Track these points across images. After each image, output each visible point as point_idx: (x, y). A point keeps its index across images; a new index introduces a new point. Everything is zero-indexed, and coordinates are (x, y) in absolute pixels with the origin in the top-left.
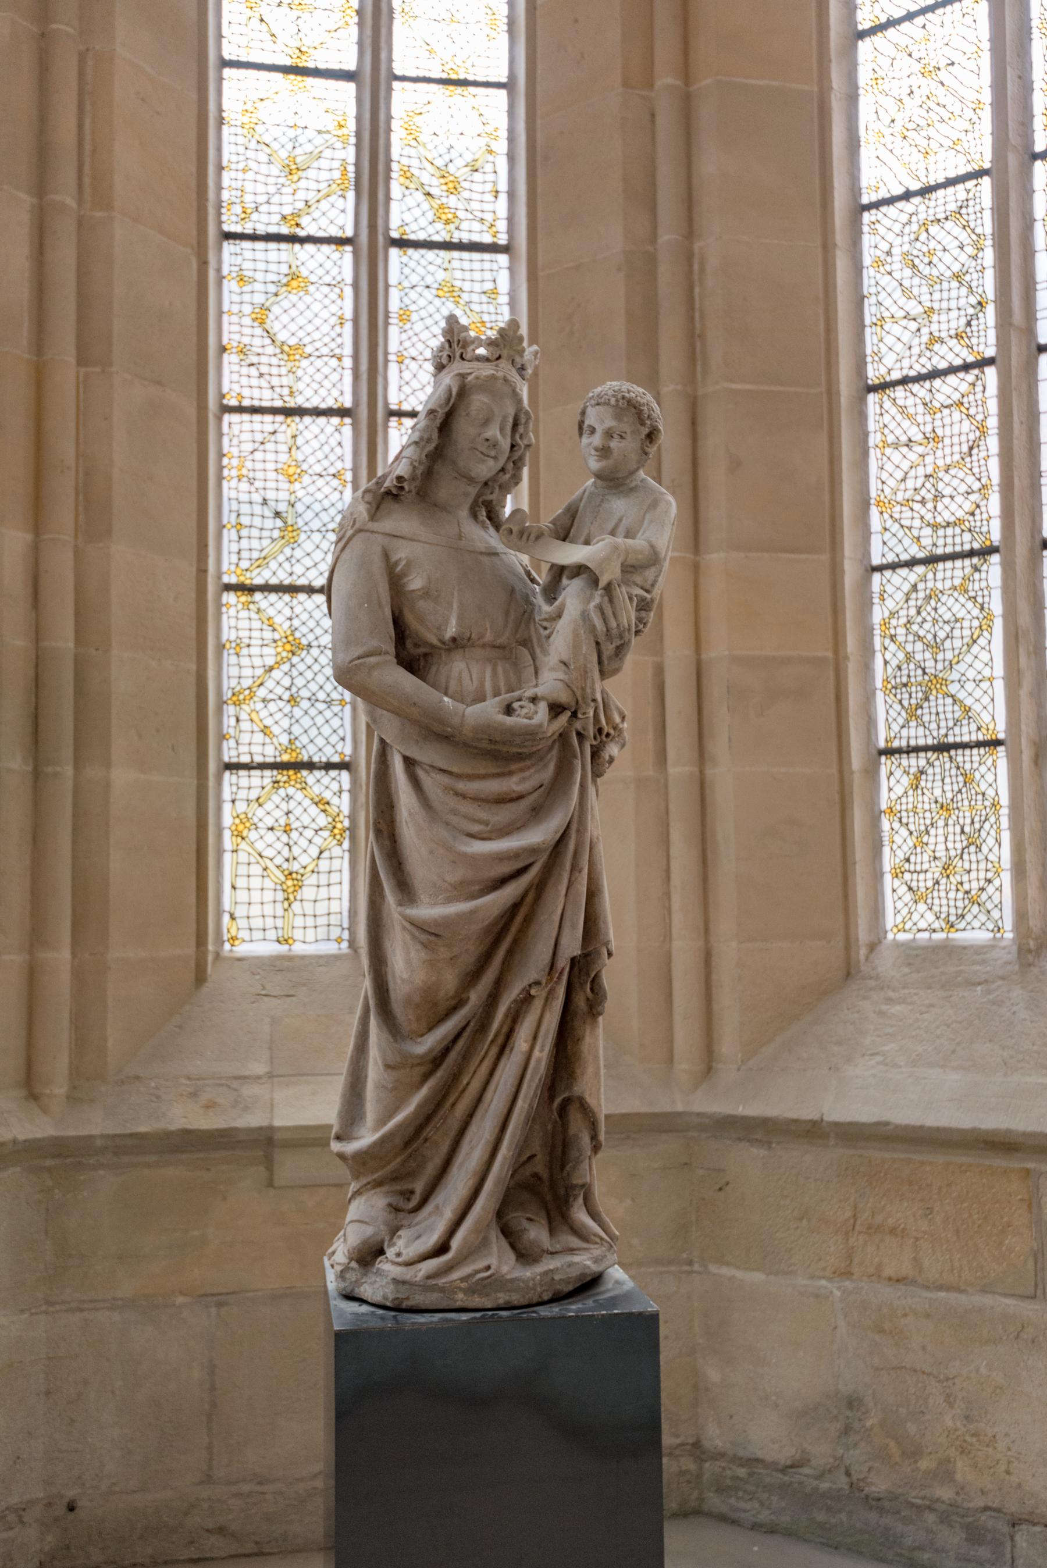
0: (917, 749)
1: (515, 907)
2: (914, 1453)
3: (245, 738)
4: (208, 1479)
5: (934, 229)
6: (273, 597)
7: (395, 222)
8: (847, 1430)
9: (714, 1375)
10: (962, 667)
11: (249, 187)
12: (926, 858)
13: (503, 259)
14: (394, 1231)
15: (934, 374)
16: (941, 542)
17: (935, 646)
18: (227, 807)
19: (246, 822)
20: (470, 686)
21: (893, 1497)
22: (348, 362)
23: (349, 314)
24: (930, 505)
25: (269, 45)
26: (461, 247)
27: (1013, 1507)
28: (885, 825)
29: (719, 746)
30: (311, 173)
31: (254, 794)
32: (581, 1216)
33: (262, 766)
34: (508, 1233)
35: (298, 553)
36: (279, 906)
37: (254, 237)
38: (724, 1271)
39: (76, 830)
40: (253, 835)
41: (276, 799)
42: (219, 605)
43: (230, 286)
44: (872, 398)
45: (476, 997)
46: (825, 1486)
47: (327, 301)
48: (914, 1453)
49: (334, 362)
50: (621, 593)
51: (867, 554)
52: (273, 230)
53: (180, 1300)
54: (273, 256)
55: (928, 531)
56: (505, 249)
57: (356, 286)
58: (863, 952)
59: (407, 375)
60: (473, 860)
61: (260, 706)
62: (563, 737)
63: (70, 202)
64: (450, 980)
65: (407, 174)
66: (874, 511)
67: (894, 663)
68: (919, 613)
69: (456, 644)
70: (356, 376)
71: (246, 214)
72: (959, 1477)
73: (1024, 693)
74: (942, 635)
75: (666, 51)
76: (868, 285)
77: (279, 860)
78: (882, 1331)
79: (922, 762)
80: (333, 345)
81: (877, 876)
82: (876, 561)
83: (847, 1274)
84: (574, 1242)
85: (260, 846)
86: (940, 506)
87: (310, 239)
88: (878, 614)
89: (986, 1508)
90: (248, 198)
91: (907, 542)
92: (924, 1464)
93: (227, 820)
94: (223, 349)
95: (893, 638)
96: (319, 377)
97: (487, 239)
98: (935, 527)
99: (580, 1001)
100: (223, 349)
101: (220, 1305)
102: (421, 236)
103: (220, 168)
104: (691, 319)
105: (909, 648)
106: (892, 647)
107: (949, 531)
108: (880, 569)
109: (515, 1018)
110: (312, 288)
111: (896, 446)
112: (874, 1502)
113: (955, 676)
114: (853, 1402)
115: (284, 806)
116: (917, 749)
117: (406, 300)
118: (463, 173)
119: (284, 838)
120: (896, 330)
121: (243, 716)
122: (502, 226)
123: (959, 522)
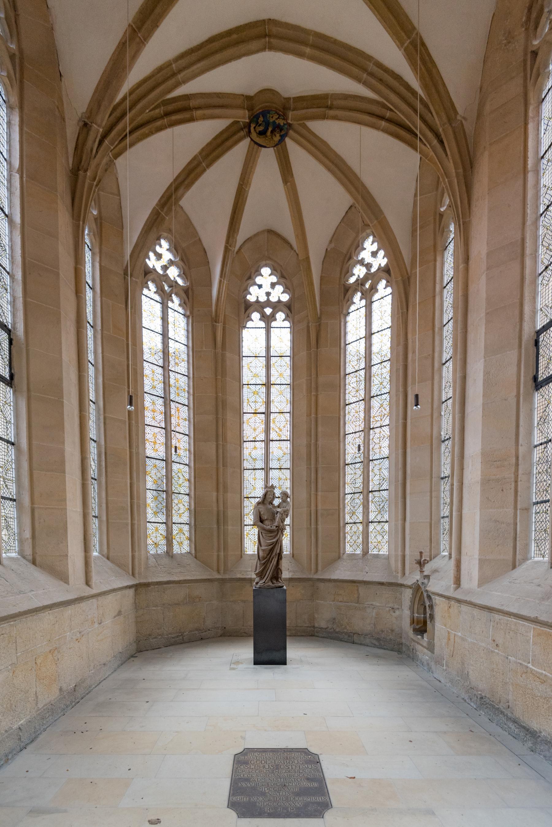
0: (351, 523)
1: (272, 548)
4: (243, 626)
5: (356, 439)
6: (252, 499)
7: (271, 437)
8: (334, 623)
9: (316, 616)
11: (248, 433)
13: (289, 442)
15: (356, 463)
17: (354, 507)
18: (245, 531)
20: (268, 524)
21: (339, 632)
22: (263, 461)
23: (264, 453)
25: (251, 409)
26: (282, 440)
27: (354, 632)
28: (346, 535)
29: (319, 523)
30: (258, 430)
32: (280, 580)
33: (250, 525)
34: (272, 582)
35: (256, 492)
37: (249, 441)
38: (318, 601)
39: (224, 535)
40: (249, 536)
42: (244, 500)
43: (245, 449)
44: (347, 466)
45: (268, 557)
50: (283, 514)
51: (345, 492)
52: (252, 440)
54: (252, 444)
56: (289, 440)
57: (265, 448)
58: (342, 555)
60: (268, 543)
62: (278, 529)
63: (221, 443)
64: (265, 555)
65: (273, 429)
66: (346, 485)
69: (266, 519)
70: (265, 463)
73: (365, 516)
75: (313, 410)
76: (346, 448)
81: (345, 543)
82: (346, 493)
83: (334, 601)
87: (258, 441)
88: (346, 501)
90: (248, 435)
93: (245, 533)
97: (286, 439)
98: (355, 488)
99: (280, 558)
102: (275, 439)
103: (243, 430)
104: (316, 455)
108: (347, 494)
109: (272, 559)
111: (350, 474)
112: (337, 633)
114: (334, 619)
116: (351, 523)
118: (282, 428)
120: (350, 455)
122: (289, 436)
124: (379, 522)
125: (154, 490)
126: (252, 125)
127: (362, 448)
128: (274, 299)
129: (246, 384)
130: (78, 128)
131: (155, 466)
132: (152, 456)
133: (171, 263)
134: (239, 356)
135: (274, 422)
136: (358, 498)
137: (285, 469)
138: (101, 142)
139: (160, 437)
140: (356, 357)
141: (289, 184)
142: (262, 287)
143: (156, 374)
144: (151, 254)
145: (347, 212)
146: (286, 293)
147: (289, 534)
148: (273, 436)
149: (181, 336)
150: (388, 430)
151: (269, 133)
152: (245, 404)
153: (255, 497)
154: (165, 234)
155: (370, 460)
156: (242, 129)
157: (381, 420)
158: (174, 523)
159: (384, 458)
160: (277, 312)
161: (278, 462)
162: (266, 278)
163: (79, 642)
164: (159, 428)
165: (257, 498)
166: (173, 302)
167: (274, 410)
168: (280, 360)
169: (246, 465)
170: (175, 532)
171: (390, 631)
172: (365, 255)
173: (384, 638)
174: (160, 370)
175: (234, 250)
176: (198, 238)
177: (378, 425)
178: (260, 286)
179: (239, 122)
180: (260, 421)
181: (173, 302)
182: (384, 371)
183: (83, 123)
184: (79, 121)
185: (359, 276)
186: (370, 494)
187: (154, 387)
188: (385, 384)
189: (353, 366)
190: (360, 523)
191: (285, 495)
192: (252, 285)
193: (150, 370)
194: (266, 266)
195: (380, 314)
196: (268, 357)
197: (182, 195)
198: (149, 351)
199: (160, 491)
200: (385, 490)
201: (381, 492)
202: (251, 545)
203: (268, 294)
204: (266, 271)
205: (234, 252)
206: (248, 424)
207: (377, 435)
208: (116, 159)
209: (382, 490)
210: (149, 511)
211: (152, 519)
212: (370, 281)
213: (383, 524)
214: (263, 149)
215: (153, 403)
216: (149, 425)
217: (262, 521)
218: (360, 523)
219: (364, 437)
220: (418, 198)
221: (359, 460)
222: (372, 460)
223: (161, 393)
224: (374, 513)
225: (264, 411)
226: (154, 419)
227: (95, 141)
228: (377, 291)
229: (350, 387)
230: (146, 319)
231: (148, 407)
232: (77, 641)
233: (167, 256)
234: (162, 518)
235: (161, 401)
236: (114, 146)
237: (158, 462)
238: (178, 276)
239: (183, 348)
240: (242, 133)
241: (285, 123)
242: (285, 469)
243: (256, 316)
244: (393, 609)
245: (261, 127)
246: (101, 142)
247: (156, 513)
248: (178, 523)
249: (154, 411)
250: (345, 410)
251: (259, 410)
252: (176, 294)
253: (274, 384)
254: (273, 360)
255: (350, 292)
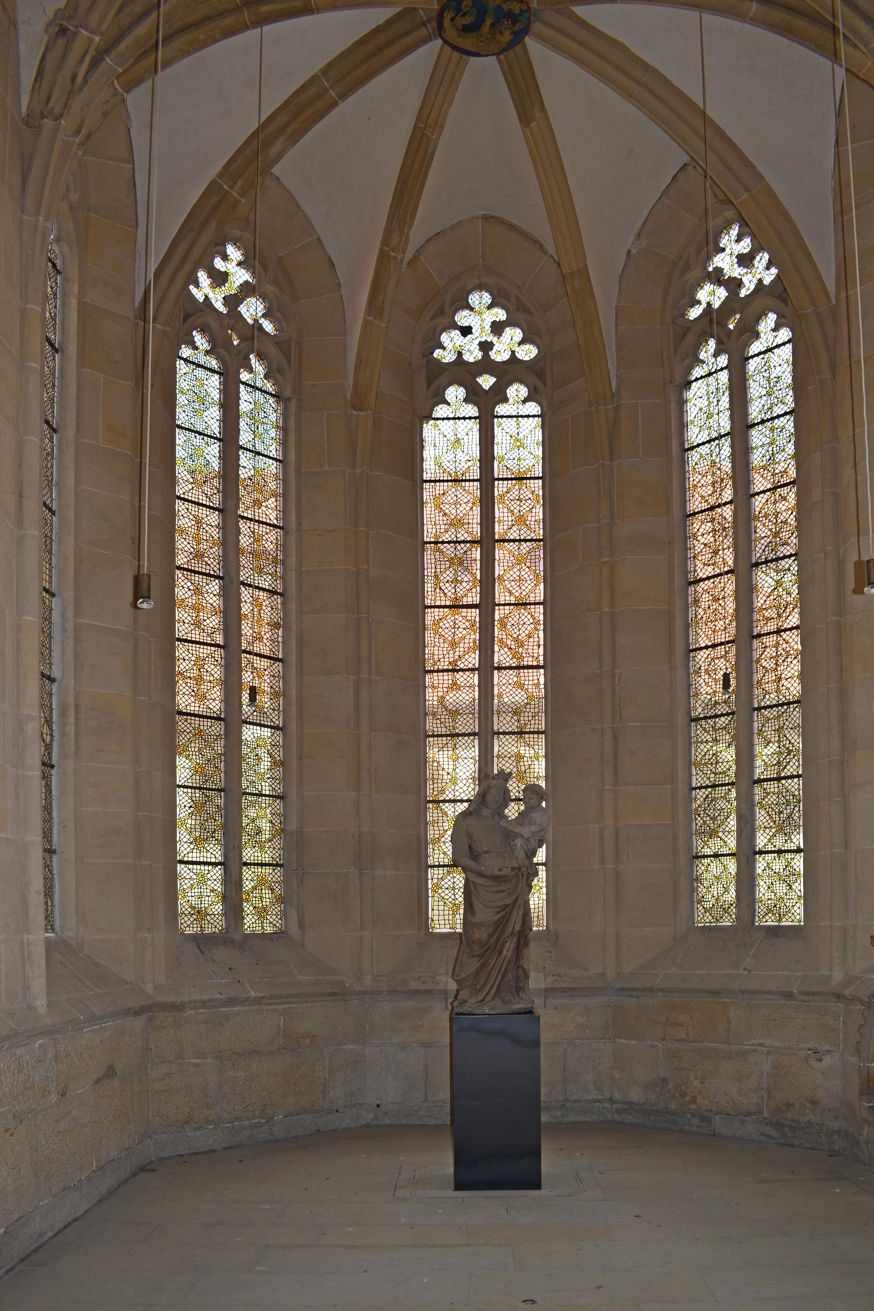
1: (502, 918)
2: (683, 1095)
3: (436, 856)
10: (724, 826)
11: (436, 652)
12: (710, 896)
14: (470, 998)
15: (716, 716)
16: (717, 780)
17: (714, 819)
18: (430, 881)
19: (437, 886)
24: (714, 766)
25: (443, 598)
30: (461, 645)
31: (440, 876)
33: (443, 866)
35: (457, 788)
36: (450, 916)
41: (449, 878)
46: (654, 1108)
47: (468, 693)
48: (683, 1095)
49: (471, 716)
53: (414, 1045)
55: (713, 775)
59: (501, 719)
61: (442, 844)
65: (501, 641)
67: (699, 824)
68: (708, 806)
71: (435, 663)
72: (698, 1102)
74: (717, 814)
77: (450, 900)
78: (675, 1057)
79: (709, 861)
80: (470, 709)
83: (664, 1039)
84: (520, 1001)
85: (443, 895)
86: (718, 766)
87: (462, 670)
89: (707, 1110)
91: (705, 779)
92: (687, 1098)
93: (430, 886)
94: (426, 714)
95: (699, 815)
96: (465, 722)
98: (716, 774)
99: (522, 941)
100: (426, 714)
101: (429, 1047)
105: (705, 819)
106: (699, 819)
107: (721, 776)
108: (695, 789)
110: (462, 689)
113: (721, 830)
114: (664, 1080)
115: (452, 880)
117: (501, 690)
119: (453, 892)
121: (436, 848)
122: (541, 658)
123: (725, 772)
124: (780, 852)
125: (195, 788)
126: (445, 14)
127: (733, 682)
128: (500, 354)
129: (430, 543)
130: (46, 38)
131: (199, 733)
132: (191, 709)
133: (246, 290)
134: (413, 480)
135: (503, 625)
136: (724, 798)
137: (534, 733)
138: (96, 62)
139: (212, 667)
140: (709, 477)
141: (534, 124)
142: (471, 333)
143: (204, 526)
144: (202, 276)
145: (675, 176)
146: (531, 342)
147: (544, 884)
148: (501, 656)
149: (268, 442)
150: (798, 639)
151: (486, 27)
152: (429, 587)
153: (455, 801)
154: (237, 233)
155: (755, 709)
156: (424, 24)
157: (779, 616)
158: (246, 864)
159: (789, 703)
160: (510, 384)
161: (516, 718)
162: (480, 313)
163: (11, 1136)
164: (211, 645)
165: (462, 801)
166: (251, 370)
167: (502, 598)
168: (517, 487)
169: (431, 725)
170: (248, 885)
171: (808, 1105)
172: (724, 262)
173: (793, 1120)
174: (214, 518)
175: (402, 260)
176: (315, 237)
177: (772, 627)
178: (466, 331)
179: (415, 9)
180: (467, 624)
181: (251, 370)
182: (782, 506)
183: (58, 28)
184: (50, 24)
185: (709, 304)
186: (757, 790)
187: (199, 555)
188: (784, 535)
189: (702, 497)
190: (729, 855)
191: (532, 790)
192: (445, 329)
193: (191, 517)
194: (480, 288)
195: (764, 383)
196: (487, 480)
197: (280, 156)
198: (189, 477)
199: (212, 790)
200: (792, 777)
201: (783, 782)
202: (446, 913)
203: (486, 347)
204: (479, 299)
205: (401, 263)
206: (436, 632)
207: (770, 652)
208: (128, 92)
209: (785, 778)
210: (182, 835)
211: (190, 855)
212: (738, 316)
213: (789, 856)
214: (472, 59)
215: (198, 591)
216: (186, 641)
217: (474, 855)
218: (729, 855)
219: (737, 655)
220: (850, 146)
221: (725, 709)
222: (759, 709)
223: (213, 564)
224: (767, 831)
225: (477, 600)
226: (199, 627)
227: (82, 61)
228: (757, 336)
229: (696, 543)
230: (185, 408)
231: (183, 601)
232: (8, 1134)
233: (240, 276)
234: (214, 853)
235: (215, 586)
236: (125, 67)
237: (208, 723)
238: (264, 316)
239: (272, 467)
240: (423, 32)
241: (525, 8)
242: (534, 733)
243: (455, 393)
244: (816, 1052)
245: (467, 18)
246: (96, 62)
247: (198, 842)
248: (254, 864)
249: (197, 608)
250: (687, 595)
251: (465, 599)
252: (260, 357)
253: (504, 541)
254: (500, 488)
255: (690, 338)
